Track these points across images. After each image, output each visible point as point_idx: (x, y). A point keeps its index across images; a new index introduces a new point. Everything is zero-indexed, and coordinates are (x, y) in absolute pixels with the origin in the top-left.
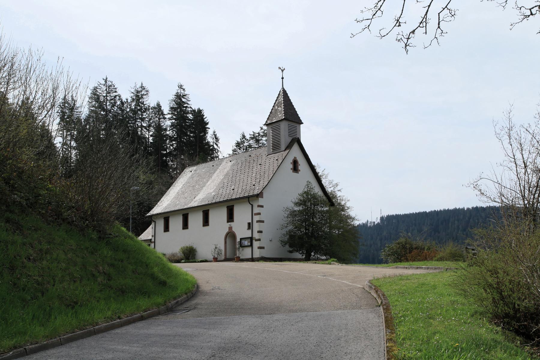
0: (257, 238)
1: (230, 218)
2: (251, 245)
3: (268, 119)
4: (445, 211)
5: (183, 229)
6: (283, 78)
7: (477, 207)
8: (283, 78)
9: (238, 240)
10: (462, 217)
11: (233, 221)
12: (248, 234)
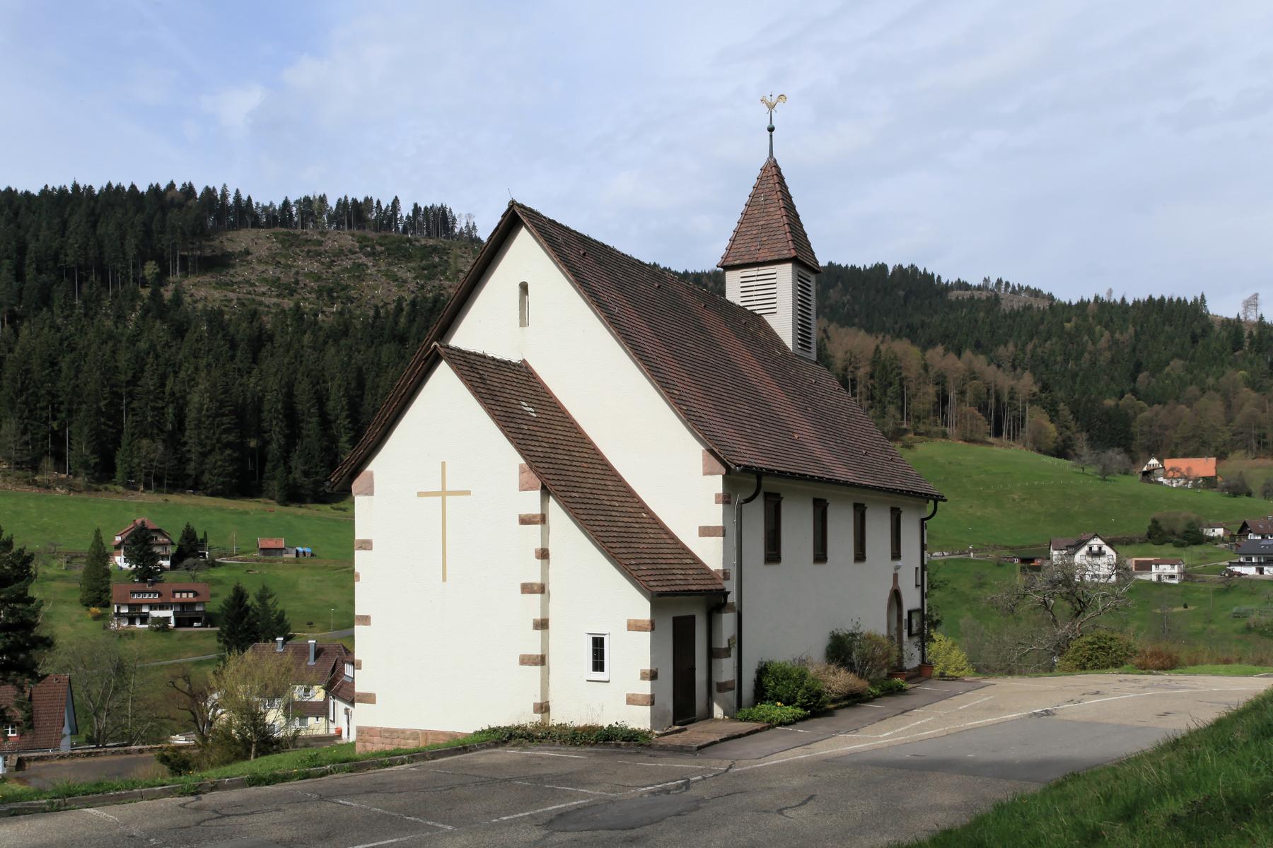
6: (771, 130)
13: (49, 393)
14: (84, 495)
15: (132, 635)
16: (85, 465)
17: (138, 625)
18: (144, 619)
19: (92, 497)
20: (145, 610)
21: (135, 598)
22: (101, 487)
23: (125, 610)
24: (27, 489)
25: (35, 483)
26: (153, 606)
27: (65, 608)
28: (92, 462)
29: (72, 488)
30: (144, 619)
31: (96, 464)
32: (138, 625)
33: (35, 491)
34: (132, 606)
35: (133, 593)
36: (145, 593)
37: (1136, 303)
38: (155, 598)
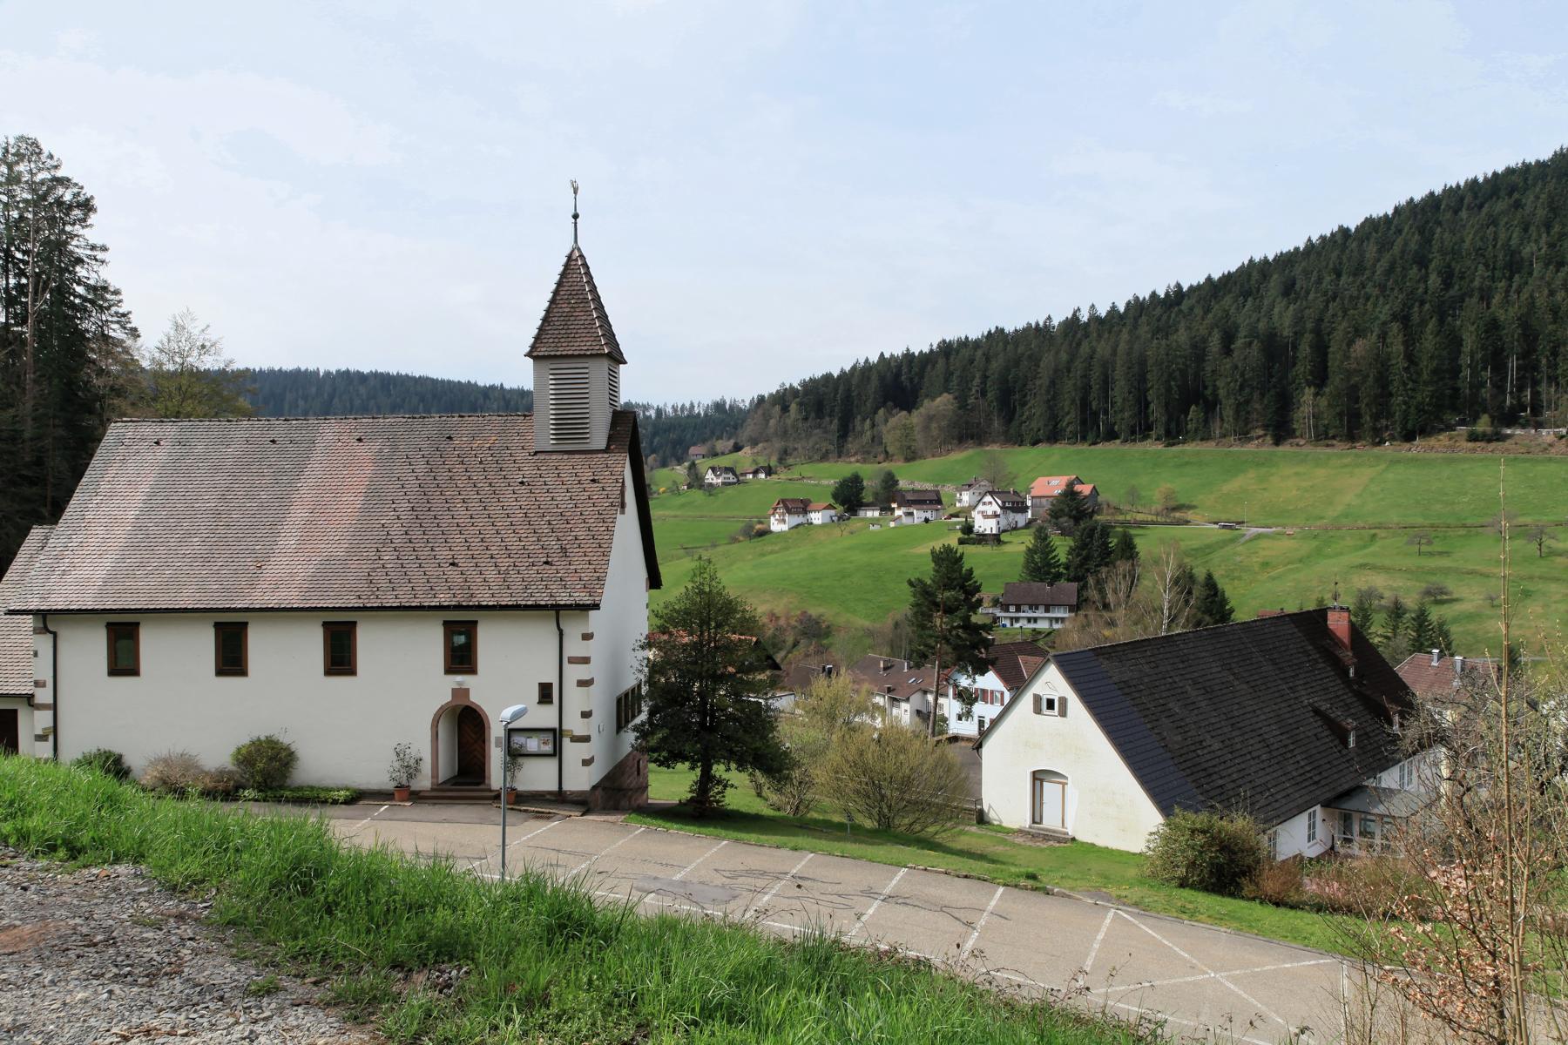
0: (577, 733)
1: (461, 659)
2: (557, 752)
3: (537, 338)
4: (272, 372)
5: (220, 672)
6: (576, 216)
7: (348, 371)
8: (576, 216)
9: (496, 731)
10: (314, 390)
11: (472, 670)
12: (546, 717)
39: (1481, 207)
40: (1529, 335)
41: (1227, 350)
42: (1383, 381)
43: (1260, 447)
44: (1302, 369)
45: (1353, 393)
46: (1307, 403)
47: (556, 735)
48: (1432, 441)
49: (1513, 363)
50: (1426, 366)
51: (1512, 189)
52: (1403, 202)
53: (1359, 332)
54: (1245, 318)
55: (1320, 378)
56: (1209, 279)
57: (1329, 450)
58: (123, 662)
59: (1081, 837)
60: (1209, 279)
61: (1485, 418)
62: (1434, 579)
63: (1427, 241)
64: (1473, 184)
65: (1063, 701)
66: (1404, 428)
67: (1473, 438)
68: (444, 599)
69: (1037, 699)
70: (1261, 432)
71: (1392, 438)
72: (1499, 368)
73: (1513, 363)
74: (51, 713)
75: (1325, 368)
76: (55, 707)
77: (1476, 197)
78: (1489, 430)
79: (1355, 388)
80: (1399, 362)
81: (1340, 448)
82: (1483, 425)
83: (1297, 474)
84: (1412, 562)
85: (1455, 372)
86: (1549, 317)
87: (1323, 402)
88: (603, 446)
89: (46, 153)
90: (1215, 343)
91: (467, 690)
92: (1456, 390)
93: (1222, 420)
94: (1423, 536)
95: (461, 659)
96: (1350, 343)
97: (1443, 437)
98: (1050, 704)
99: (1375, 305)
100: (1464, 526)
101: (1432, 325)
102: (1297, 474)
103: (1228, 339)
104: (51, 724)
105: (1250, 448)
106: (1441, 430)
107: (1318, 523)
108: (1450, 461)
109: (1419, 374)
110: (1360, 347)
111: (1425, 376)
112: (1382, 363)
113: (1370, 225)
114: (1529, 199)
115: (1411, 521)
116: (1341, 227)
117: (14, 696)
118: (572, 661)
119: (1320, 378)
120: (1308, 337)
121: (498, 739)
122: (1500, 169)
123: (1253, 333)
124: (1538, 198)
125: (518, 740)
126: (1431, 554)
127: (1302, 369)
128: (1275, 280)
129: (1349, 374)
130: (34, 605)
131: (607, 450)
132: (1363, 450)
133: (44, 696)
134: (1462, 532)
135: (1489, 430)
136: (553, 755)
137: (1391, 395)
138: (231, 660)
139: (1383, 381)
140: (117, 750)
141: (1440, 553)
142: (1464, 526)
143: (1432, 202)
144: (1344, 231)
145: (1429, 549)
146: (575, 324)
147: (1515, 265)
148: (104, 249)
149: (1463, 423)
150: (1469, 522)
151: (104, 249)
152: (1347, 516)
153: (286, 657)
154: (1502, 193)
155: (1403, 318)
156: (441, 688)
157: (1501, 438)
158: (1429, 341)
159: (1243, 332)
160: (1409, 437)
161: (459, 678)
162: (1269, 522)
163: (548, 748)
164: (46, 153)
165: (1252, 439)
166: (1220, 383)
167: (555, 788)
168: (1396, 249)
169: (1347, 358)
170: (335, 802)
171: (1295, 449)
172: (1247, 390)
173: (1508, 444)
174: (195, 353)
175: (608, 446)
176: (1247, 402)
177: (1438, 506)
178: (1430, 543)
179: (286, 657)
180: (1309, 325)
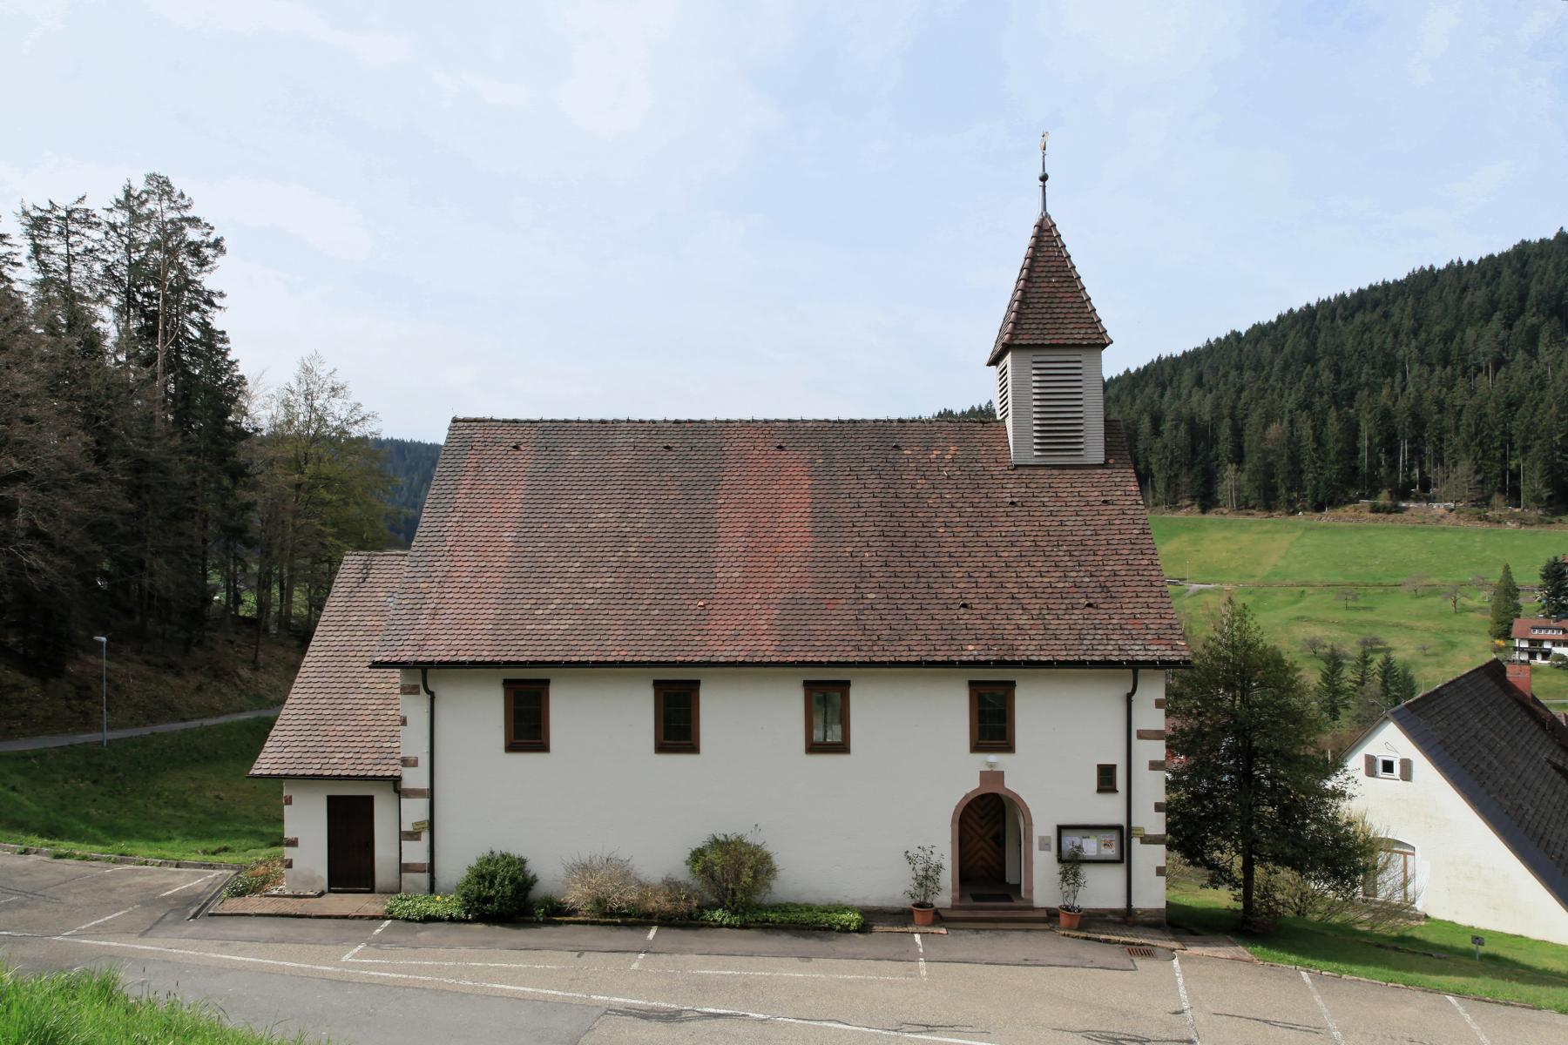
1: (992, 727)
5: (661, 748)
6: (1044, 178)
9: (1042, 826)
11: (1009, 747)
12: (1109, 810)
13: (1503, 433)
14: (1535, 529)
15: (1535, 670)
16: (1537, 499)
17: (1539, 660)
18: (1546, 655)
19: (1542, 530)
20: (1547, 646)
21: (1536, 634)
22: (1555, 519)
23: (1525, 645)
24: (1479, 524)
25: (1487, 519)
26: (1555, 643)
27: (1474, 639)
28: (1545, 496)
29: (1523, 522)
30: (1546, 655)
31: (1550, 497)
32: (1539, 660)
33: (1486, 526)
34: (1533, 642)
35: (1534, 628)
36: (1547, 629)
37: (1352, 295)
38: (1560, 635)
39: (1352, 316)
40: (1418, 422)
41: (1156, 430)
42: (1295, 459)
43: (1188, 515)
44: (1224, 447)
45: (1268, 472)
46: (1230, 478)
47: (1125, 834)
48: (1340, 512)
49: (1405, 447)
50: (1332, 448)
51: (1376, 304)
52: (1285, 312)
53: (1269, 418)
54: (1168, 405)
55: (1239, 457)
56: (1128, 372)
57: (1249, 518)
58: (527, 730)
59: (1433, 914)
60: (1128, 372)
61: (1384, 494)
62: (1365, 631)
63: (1313, 344)
64: (1342, 298)
65: (1406, 765)
66: (1315, 500)
67: (1375, 509)
68: (972, 651)
69: (1370, 761)
70: (1188, 502)
71: (1304, 509)
72: (1392, 452)
73: (1405, 447)
74: (425, 802)
75: (1241, 448)
76: (431, 794)
77: (1345, 309)
78: (1389, 503)
79: (1271, 465)
80: (1308, 444)
81: (1259, 516)
82: (1383, 498)
83: (1225, 538)
84: (1340, 616)
85: (1354, 452)
86: (1434, 408)
87: (1244, 477)
88: (1100, 459)
89: (177, 193)
90: (1145, 425)
91: (1001, 774)
92: (1355, 469)
93: (1154, 488)
94: (1351, 593)
95: (992, 727)
96: (1265, 427)
97: (1349, 508)
98: (1388, 766)
99: (1282, 396)
100: (1380, 585)
101: (1333, 414)
102: (1225, 538)
103: (1157, 421)
104: (426, 817)
105: (1181, 514)
106: (1346, 503)
107: (1251, 581)
108: (1358, 529)
109: (1326, 453)
110: (1274, 430)
111: (1332, 456)
112: (1293, 442)
113: (1259, 332)
114: (1396, 310)
115: (1333, 580)
116: (1233, 332)
117: (374, 778)
118: (1142, 735)
119: (1239, 457)
120: (1227, 422)
121: (1042, 839)
122: (1365, 286)
123: (1179, 418)
124: (1403, 310)
125: (1070, 840)
126: (1357, 609)
127: (1224, 447)
128: (1188, 375)
129: (1266, 454)
130: (407, 655)
131: (1105, 466)
132: (1279, 519)
133: (415, 778)
134: (1380, 590)
135: (1389, 503)
136: (1119, 861)
137: (1302, 472)
138: (677, 729)
139: (1295, 459)
140: (516, 852)
141: (1364, 608)
142: (1380, 585)
143: (1309, 313)
144: (1236, 335)
145: (1354, 604)
146: (1049, 309)
147: (1390, 366)
148: (221, 295)
149: (1362, 496)
150: (1384, 581)
151: (221, 295)
152: (1275, 574)
153: (751, 726)
154: (1369, 306)
155: (1306, 406)
156: (964, 772)
157: (1401, 510)
158: (1333, 427)
159: (1169, 416)
160: (1319, 508)
161: (992, 758)
162: (1208, 579)
163: (1112, 852)
164: (177, 193)
165: (1181, 508)
166: (1153, 459)
167: (1120, 904)
168: (1287, 350)
169: (1264, 439)
170: (845, 930)
171: (1220, 517)
172: (1176, 466)
173: (1404, 515)
174: (325, 395)
175: (1106, 461)
176: (1176, 476)
177: (1354, 568)
178: (1355, 598)
179: (751, 726)
180: (1226, 412)
